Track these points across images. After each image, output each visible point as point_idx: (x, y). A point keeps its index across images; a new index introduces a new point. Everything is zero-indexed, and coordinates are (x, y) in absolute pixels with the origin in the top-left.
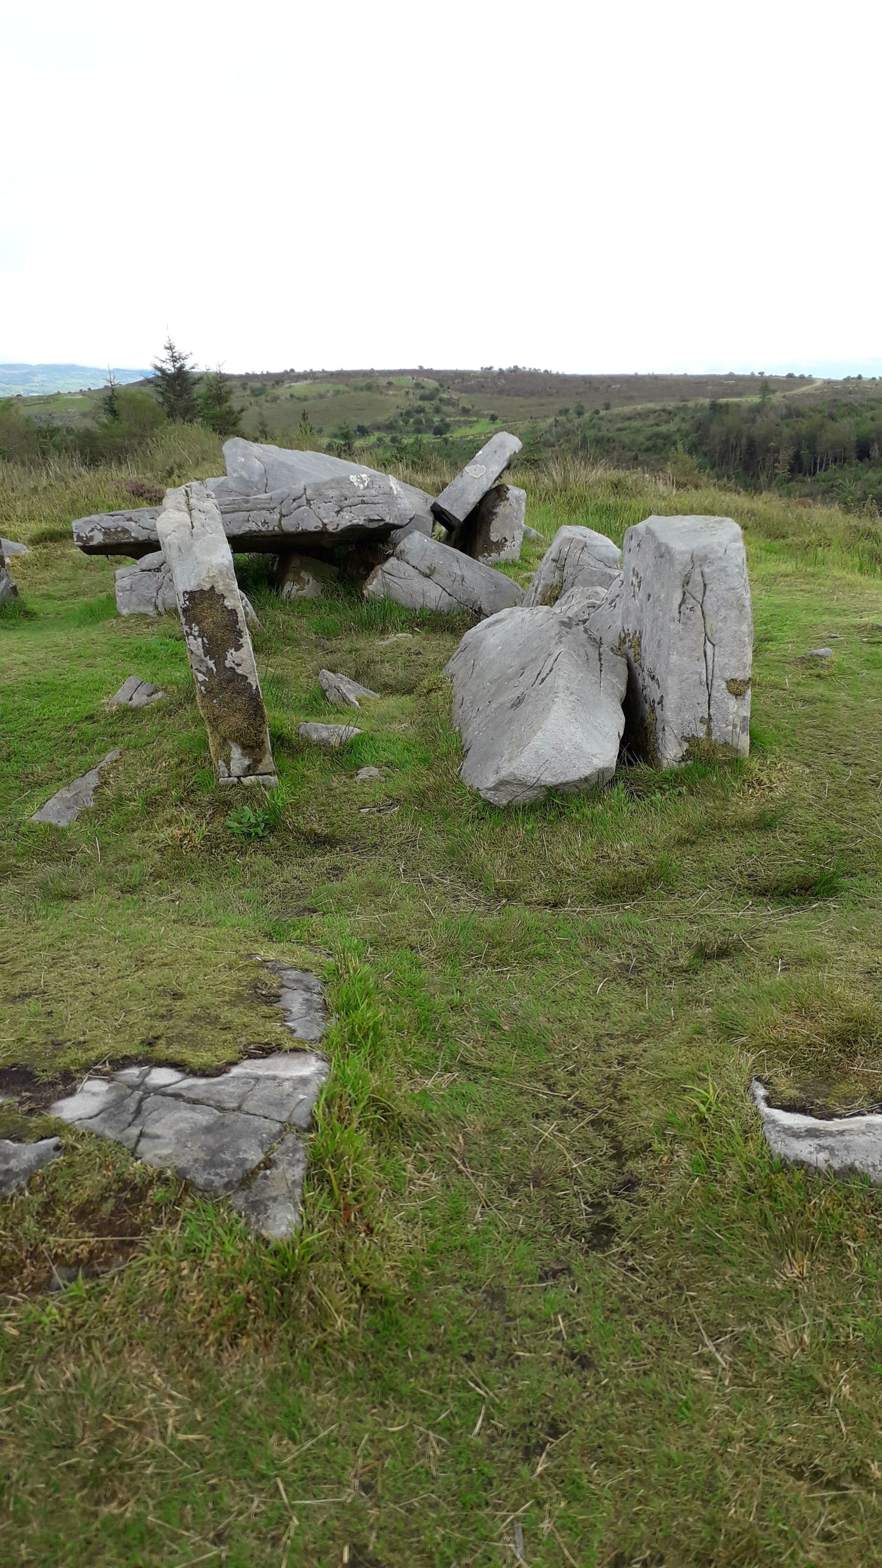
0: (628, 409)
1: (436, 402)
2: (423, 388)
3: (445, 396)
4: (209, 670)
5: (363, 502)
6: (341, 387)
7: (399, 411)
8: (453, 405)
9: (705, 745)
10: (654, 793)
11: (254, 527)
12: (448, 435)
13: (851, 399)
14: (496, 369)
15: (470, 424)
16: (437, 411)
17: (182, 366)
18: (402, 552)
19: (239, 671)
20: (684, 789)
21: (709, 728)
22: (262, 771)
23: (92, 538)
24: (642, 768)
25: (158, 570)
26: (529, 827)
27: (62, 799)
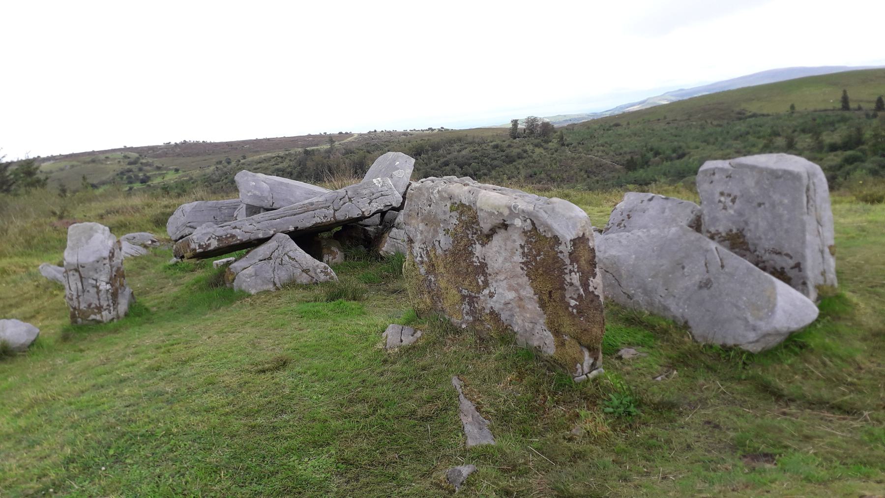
0: (256, 158)
1: (139, 165)
3: (144, 161)
4: (580, 296)
5: (382, 195)
6: (75, 163)
11: (319, 221)
12: (149, 183)
13: (375, 141)
16: (140, 170)
23: (209, 245)
25: (270, 258)
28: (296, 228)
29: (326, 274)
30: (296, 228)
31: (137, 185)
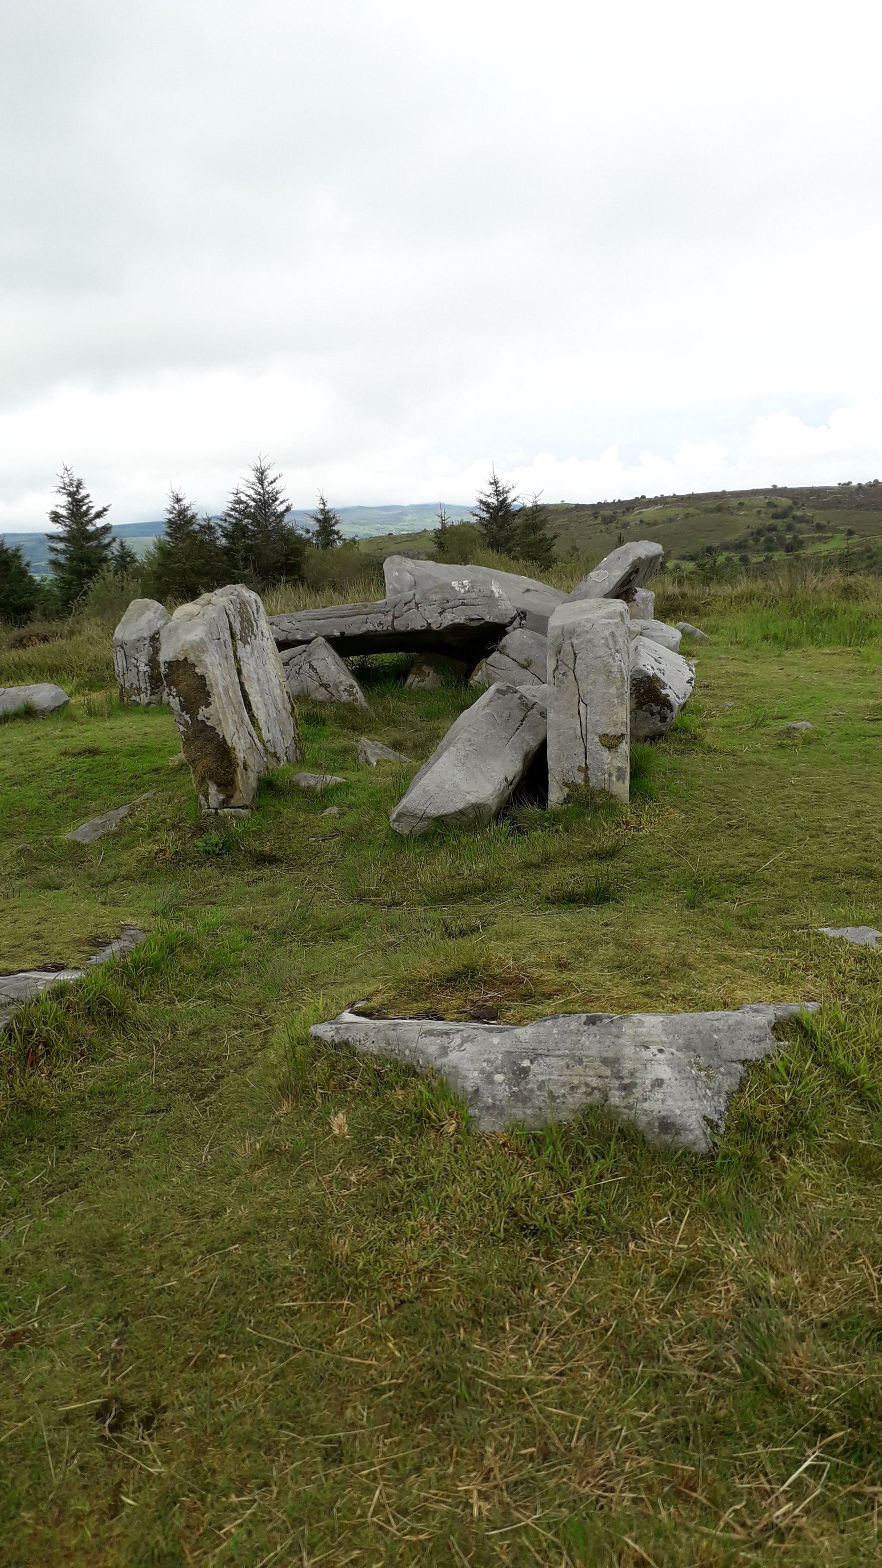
1: (788, 520)
2: (776, 506)
3: (799, 513)
5: (463, 604)
6: (692, 510)
7: (750, 530)
8: (807, 522)
9: (583, 790)
10: (536, 830)
11: (371, 628)
14: (855, 483)
15: (823, 540)
16: (790, 528)
17: (505, 499)
18: (504, 647)
19: (209, 723)
20: (561, 828)
21: (586, 776)
22: (237, 805)
24: (532, 810)
26: (418, 851)
27: (93, 824)
28: (342, 634)
29: (351, 694)
30: (342, 634)
31: (779, 555)
